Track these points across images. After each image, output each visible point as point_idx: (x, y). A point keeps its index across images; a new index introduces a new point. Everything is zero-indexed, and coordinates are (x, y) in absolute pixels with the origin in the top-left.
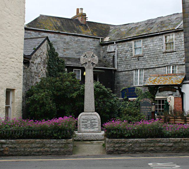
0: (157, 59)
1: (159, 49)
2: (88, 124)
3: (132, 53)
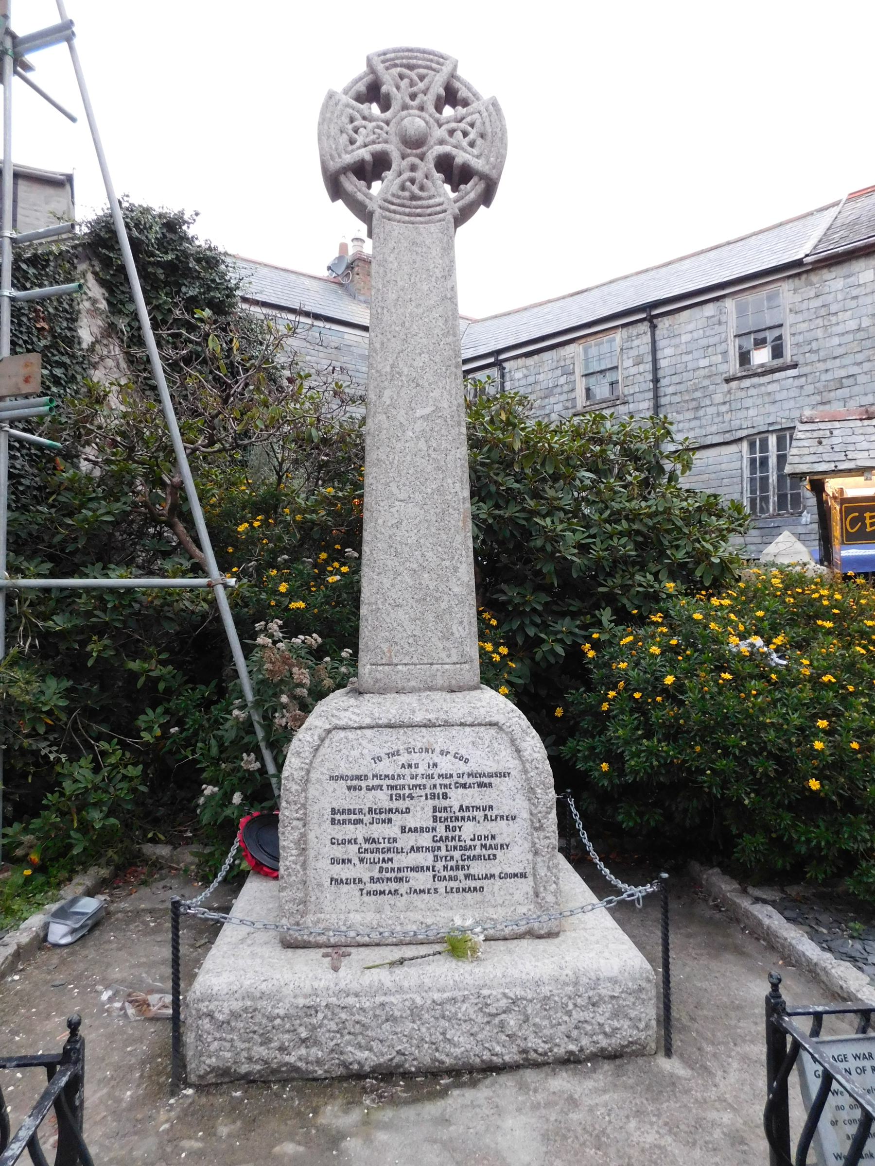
0: (697, 409)
1: (703, 363)
2: (410, 840)
3: (572, 395)
